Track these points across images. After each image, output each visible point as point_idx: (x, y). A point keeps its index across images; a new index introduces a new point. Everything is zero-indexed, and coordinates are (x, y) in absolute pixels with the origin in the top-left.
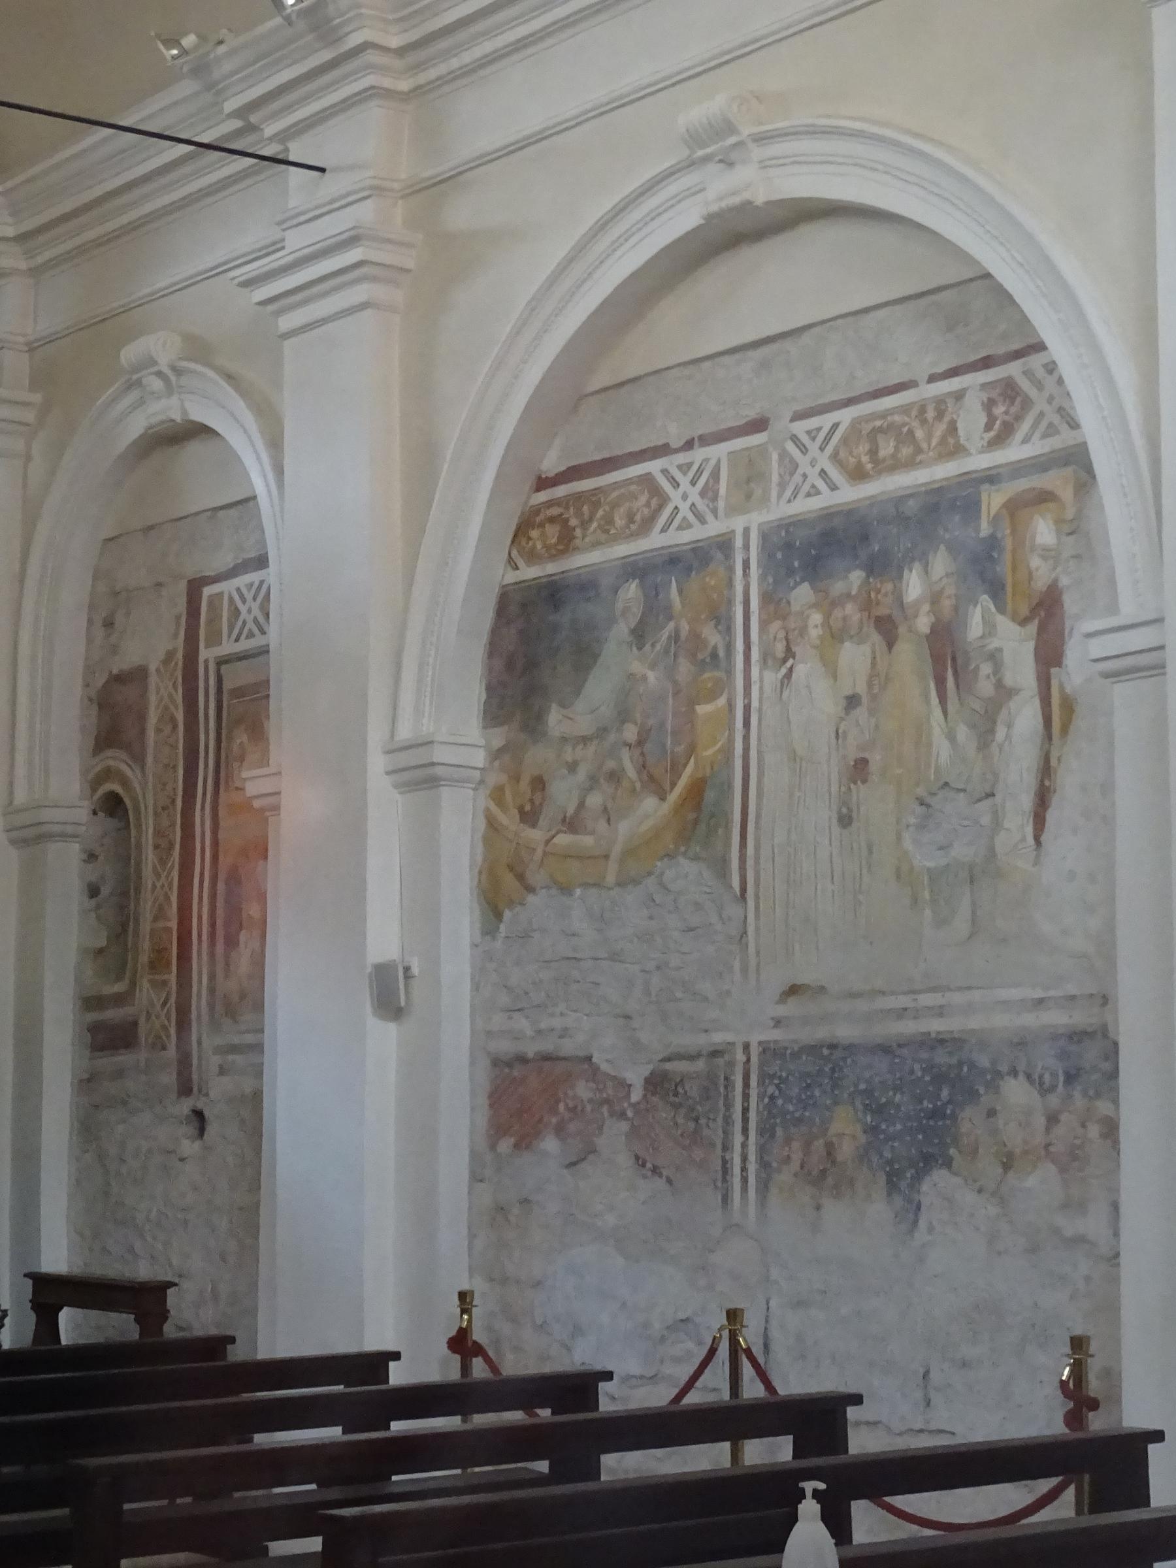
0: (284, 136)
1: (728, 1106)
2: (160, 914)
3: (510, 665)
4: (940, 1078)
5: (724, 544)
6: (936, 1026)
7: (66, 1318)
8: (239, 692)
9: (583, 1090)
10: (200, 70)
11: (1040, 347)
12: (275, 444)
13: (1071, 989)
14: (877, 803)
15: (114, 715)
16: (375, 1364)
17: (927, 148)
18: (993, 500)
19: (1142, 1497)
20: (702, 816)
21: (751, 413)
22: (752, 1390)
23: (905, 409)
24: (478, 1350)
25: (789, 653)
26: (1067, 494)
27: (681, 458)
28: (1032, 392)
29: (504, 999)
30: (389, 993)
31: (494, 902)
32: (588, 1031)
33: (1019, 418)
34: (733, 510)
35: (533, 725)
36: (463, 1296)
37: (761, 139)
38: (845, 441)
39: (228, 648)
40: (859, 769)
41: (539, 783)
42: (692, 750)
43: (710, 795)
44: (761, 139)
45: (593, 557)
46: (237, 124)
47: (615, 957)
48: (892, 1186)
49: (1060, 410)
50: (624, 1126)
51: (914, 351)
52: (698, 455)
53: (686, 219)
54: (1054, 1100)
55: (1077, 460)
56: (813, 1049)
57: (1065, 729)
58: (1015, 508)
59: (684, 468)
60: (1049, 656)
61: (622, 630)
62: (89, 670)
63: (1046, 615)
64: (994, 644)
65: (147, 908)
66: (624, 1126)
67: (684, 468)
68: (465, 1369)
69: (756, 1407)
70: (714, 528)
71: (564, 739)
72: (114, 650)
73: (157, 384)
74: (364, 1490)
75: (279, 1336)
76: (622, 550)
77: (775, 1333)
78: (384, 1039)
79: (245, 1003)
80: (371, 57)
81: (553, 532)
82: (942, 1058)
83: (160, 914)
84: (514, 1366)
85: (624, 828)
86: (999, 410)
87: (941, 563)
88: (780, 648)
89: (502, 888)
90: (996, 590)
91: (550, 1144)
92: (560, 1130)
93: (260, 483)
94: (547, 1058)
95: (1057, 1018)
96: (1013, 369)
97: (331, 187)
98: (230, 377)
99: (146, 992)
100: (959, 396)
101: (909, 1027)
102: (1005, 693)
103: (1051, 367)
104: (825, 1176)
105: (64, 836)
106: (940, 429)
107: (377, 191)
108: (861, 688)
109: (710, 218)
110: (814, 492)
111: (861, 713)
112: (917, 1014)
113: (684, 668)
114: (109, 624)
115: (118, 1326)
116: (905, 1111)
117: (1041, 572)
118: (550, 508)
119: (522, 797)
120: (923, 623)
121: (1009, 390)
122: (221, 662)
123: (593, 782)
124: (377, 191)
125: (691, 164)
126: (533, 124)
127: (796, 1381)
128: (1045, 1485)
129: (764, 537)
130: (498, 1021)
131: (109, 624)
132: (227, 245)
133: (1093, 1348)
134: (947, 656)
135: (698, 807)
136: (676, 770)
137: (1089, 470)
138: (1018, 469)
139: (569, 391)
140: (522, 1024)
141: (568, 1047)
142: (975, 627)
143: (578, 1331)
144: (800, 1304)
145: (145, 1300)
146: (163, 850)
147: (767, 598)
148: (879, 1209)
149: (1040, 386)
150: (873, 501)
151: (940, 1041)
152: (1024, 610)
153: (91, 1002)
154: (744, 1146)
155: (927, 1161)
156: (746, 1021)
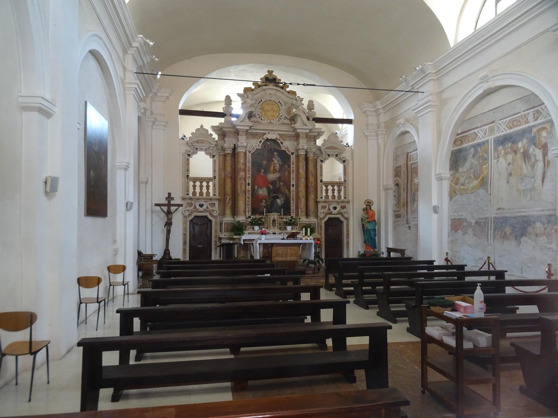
0: (418, 88)
1: (488, 226)
2: (404, 199)
3: (453, 162)
4: (525, 222)
5: (487, 141)
6: (524, 214)
7: (392, 253)
8: (414, 168)
9: (465, 224)
10: (406, 80)
11: (544, 104)
12: (418, 133)
13: (549, 208)
14: (513, 179)
15: (397, 172)
16: (432, 262)
17: (523, 74)
18: (535, 130)
19: (344, 322)
20: (484, 183)
21: (492, 120)
22: (492, 269)
23: (519, 117)
24: (449, 261)
25: (498, 157)
26: (549, 127)
27: (480, 129)
28: (542, 111)
29: (453, 211)
30: (436, 210)
31: (451, 197)
32: (464, 215)
33: (540, 116)
34: (489, 136)
35: (457, 171)
36: (447, 253)
37: (492, 77)
38: (508, 123)
39: (412, 162)
40: (510, 174)
41: (458, 179)
42: (482, 172)
43: (485, 180)
44: (492, 77)
45: (466, 145)
46: (411, 88)
47: (470, 204)
48: (516, 238)
49: (548, 114)
50: (471, 229)
51: (521, 107)
52: (483, 128)
53: (480, 92)
54: (546, 226)
55: (551, 122)
56: (502, 218)
57: (548, 166)
58: (538, 131)
59: (481, 130)
60: (545, 154)
61: (471, 156)
62: (394, 166)
63: (545, 148)
64: (534, 153)
65: (402, 198)
66: (471, 229)
67: (481, 130)
68: (447, 263)
69: (492, 271)
70: (486, 139)
71: (462, 172)
72: (397, 163)
73: (401, 126)
74: (430, 279)
75: (422, 257)
76: (471, 143)
77: (496, 261)
78: (435, 216)
79: (415, 211)
80: (430, 75)
81: (460, 142)
82: (525, 219)
83: (404, 199)
84: (454, 264)
85: (471, 185)
86: (536, 115)
87: (525, 141)
88: (497, 156)
89: (452, 194)
90: (535, 144)
91: (460, 232)
92: (461, 229)
93: (416, 138)
94: (459, 219)
95: (547, 213)
96: (539, 108)
97: (425, 94)
98: (411, 124)
99: (402, 210)
100: (528, 114)
101: (519, 214)
102: (536, 161)
103: (546, 107)
104: (504, 237)
105: (390, 189)
106: (525, 120)
107: (432, 94)
108: (511, 162)
109: (484, 91)
110: (503, 132)
111: (511, 165)
112: (520, 212)
113: (481, 160)
114: (396, 160)
115: (398, 255)
116: (518, 228)
117: (544, 141)
118: (459, 138)
119: (455, 181)
120: (522, 151)
121: (538, 111)
122: (412, 164)
123: (466, 178)
124: (432, 94)
125: (481, 83)
126: (455, 81)
127: (498, 268)
128: (543, 287)
129: (494, 139)
130: (452, 214)
131: (396, 160)
132: (411, 105)
133: (553, 266)
134: (526, 156)
135: (483, 181)
136: (479, 176)
137: (553, 123)
138: (539, 124)
139: (462, 121)
140: (456, 214)
141: (462, 217)
142: (531, 150)
143: (464, 259)
144: (500, 256)
145: (402, 252)
146: (404, 190)
147: (494, 149)
148: (514, 242)
149: (544, 110)
150: (513, 132)
151: (524, 216)
152: (540, 147)
153: (395, 211)
154: (491, 232)
155: (522, 235)
156: (491, 213)
